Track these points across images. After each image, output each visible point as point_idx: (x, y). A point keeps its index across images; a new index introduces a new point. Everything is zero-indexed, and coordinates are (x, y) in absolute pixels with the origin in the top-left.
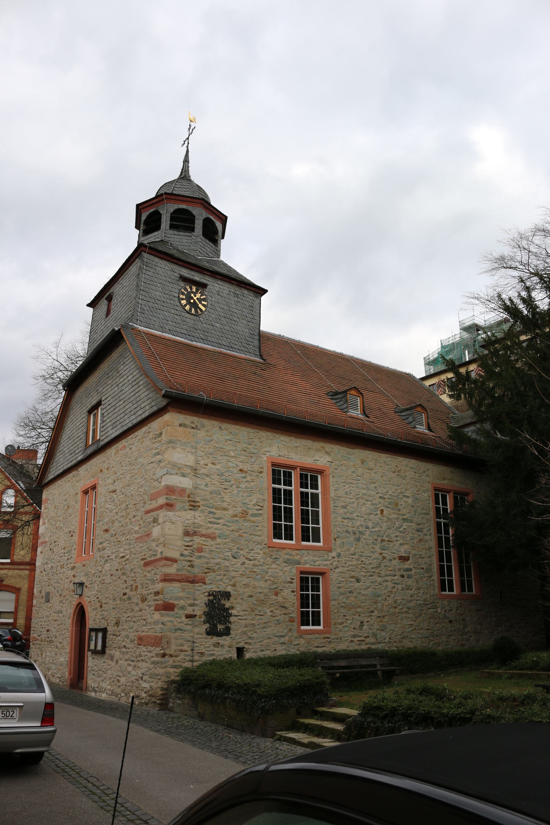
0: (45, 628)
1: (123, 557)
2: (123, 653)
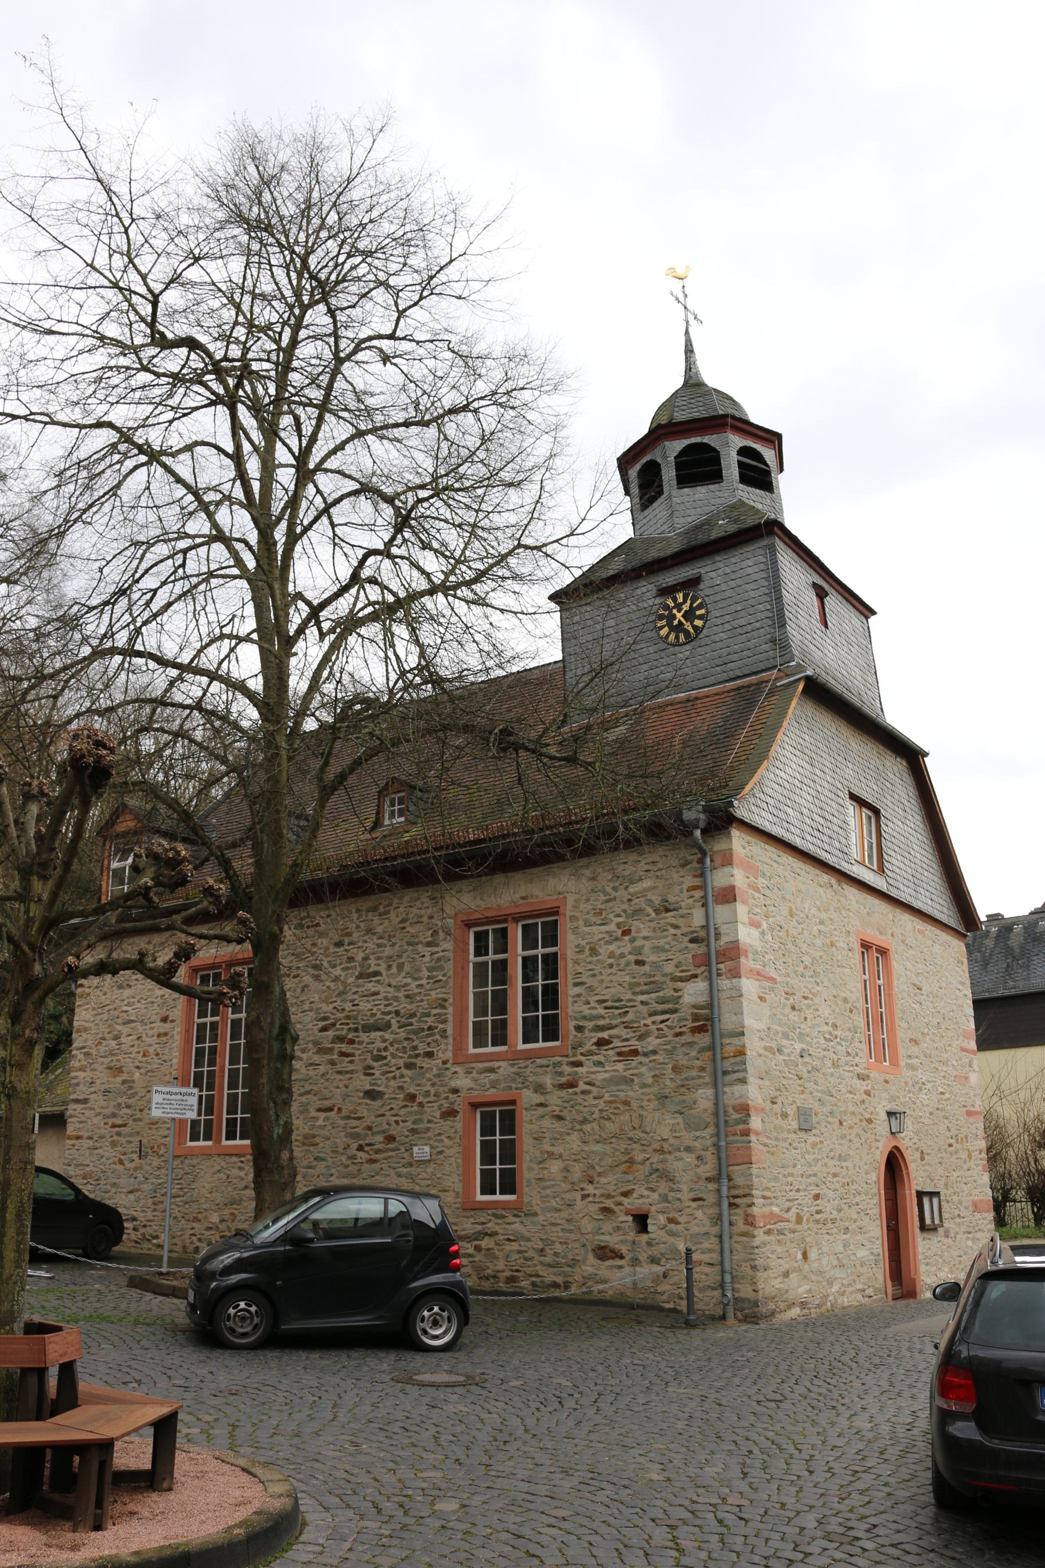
0: (805, 1190)
1: (943, 1093)
2: (959, 1224)
